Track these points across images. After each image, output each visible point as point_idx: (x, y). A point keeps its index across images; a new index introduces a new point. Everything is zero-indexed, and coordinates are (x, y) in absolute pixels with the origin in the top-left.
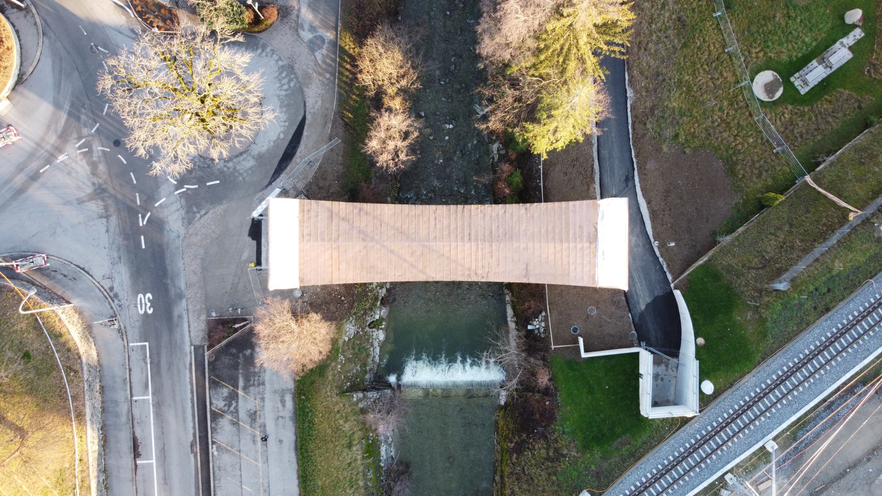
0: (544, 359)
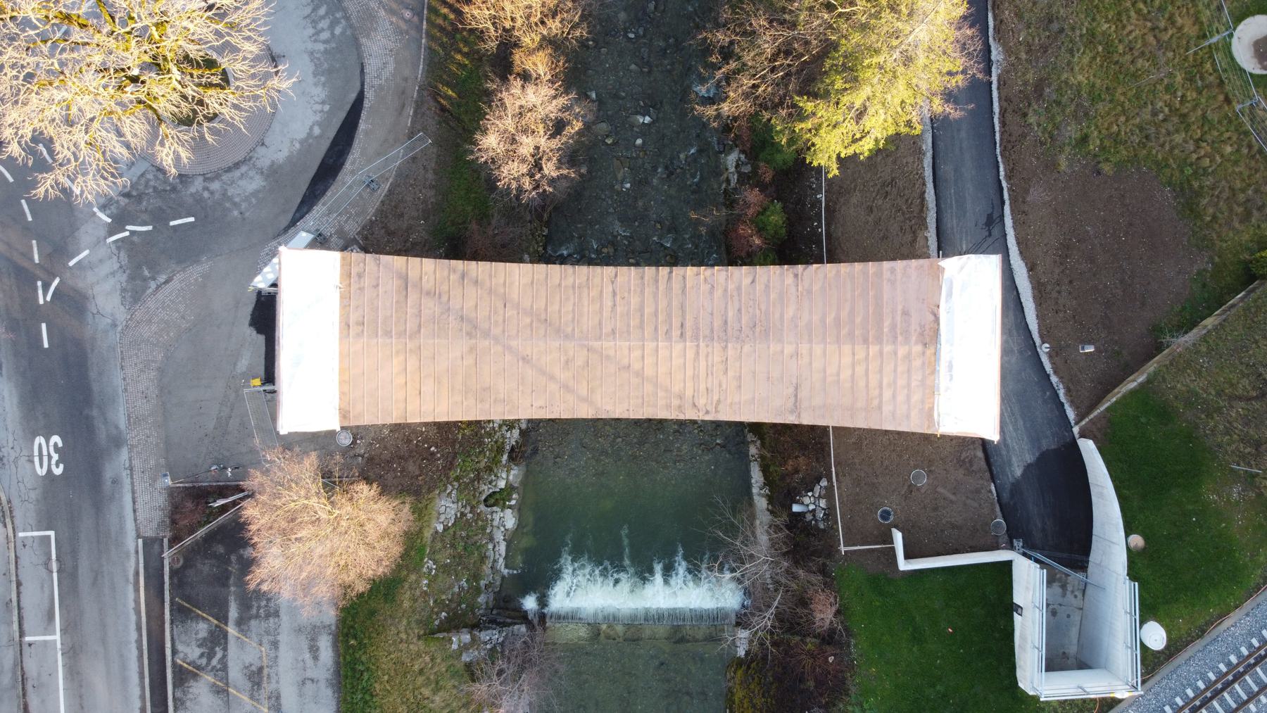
0: (823, 571)
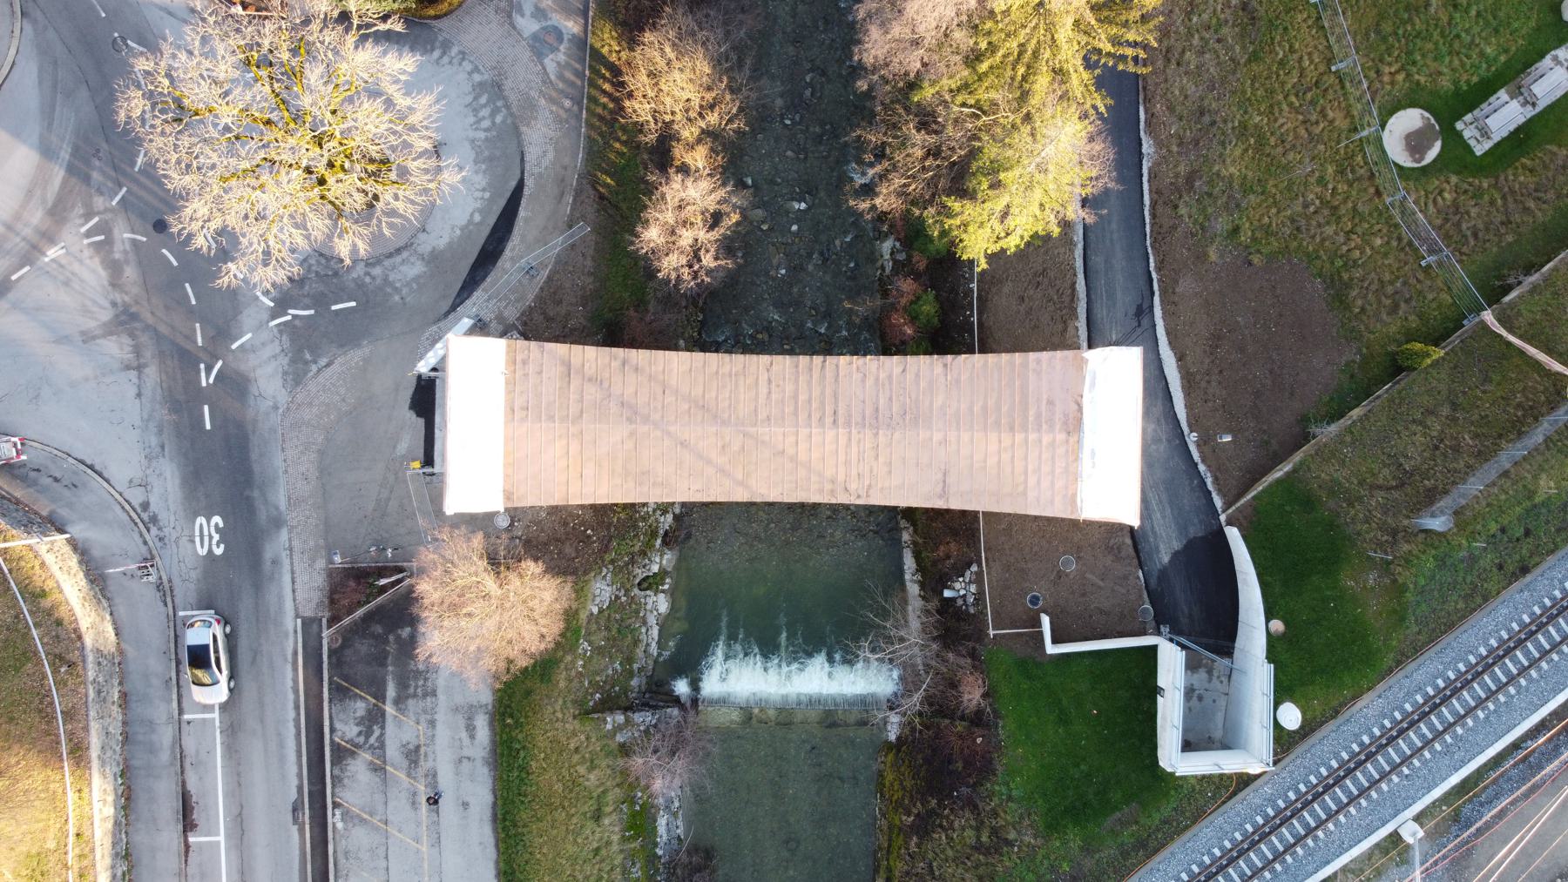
0: (973, 655)
